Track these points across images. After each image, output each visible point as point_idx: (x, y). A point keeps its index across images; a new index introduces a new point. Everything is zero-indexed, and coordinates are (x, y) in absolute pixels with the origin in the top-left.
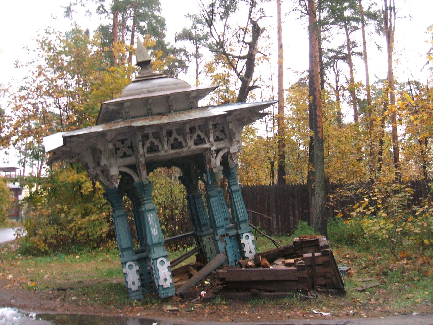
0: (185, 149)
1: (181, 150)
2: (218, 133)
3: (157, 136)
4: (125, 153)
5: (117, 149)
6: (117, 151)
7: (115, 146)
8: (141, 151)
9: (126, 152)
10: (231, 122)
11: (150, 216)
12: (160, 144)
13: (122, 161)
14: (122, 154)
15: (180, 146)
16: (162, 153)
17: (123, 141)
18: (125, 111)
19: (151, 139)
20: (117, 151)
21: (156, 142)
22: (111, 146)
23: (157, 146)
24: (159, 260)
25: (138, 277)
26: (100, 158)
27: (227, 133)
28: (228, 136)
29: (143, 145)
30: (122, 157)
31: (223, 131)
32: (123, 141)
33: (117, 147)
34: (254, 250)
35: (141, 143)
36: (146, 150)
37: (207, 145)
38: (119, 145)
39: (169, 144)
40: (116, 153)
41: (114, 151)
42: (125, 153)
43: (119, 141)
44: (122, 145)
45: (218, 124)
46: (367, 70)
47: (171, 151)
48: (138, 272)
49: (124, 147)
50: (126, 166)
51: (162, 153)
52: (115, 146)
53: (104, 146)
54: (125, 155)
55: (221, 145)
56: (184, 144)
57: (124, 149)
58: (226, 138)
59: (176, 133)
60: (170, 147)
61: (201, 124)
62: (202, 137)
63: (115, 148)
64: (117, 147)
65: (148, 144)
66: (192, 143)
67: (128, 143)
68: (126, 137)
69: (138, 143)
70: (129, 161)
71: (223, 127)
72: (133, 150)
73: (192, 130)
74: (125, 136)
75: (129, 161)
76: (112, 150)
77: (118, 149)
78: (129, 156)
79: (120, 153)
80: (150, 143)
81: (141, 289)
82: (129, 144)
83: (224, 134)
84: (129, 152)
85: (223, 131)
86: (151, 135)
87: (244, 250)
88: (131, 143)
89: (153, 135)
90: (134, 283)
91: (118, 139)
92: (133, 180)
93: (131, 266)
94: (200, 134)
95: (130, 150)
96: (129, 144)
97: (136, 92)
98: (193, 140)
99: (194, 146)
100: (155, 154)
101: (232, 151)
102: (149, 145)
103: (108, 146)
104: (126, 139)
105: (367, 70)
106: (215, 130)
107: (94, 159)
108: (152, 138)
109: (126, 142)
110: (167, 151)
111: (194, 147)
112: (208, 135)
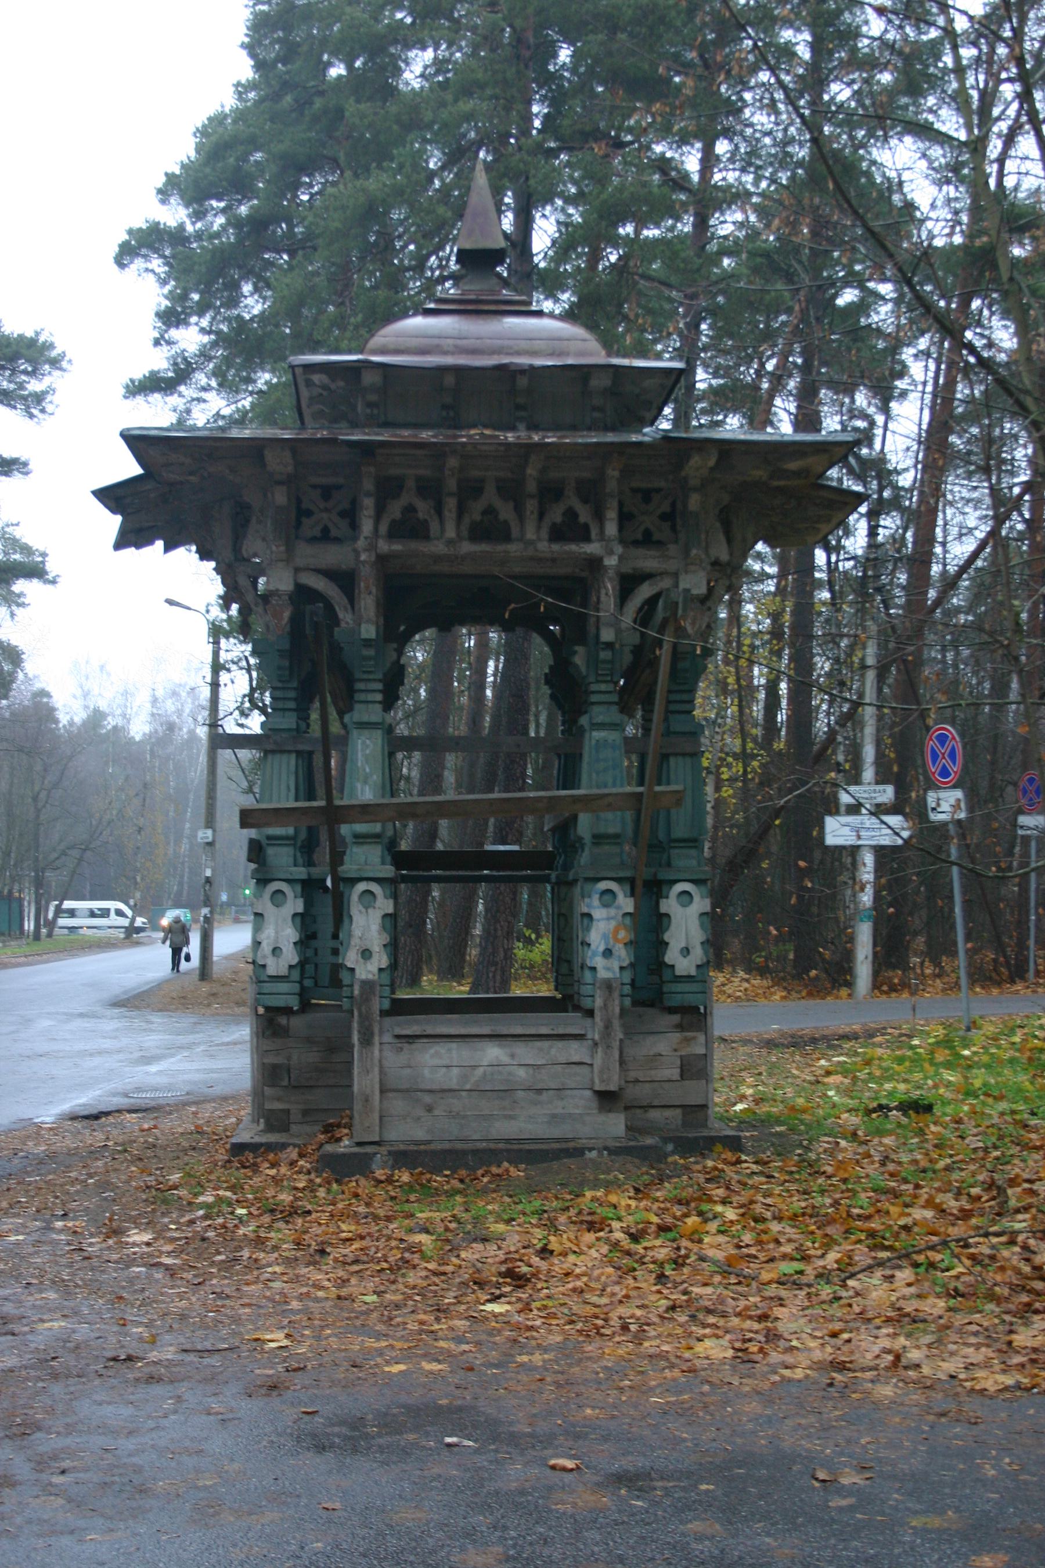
0: (513, 548)
1: (500, 548)
3: (511, 491)
4: (326, 530)
5: (303, 513)
7: (299, 501)
8: (367, 526)
9: (330, 525)
11: (364, 743)
13: (307, 554)
14: (317, 532)
16: (438, 547)
19: (490, 496)
20: (304, 520)
21: (424, 509)
23: (506, 522)
24: (362, 887)
30: (313, 540)
32: (327, 492)
33: (304, 506)
36: (383, 529)
37: (593, 548)
42: (326, 530)
43: (314, 487)
45: (658, 490)
47: (467, 547)
48: (298, 920)
49: (327, 510)
50: (318, 571)
52: (299, 501)
54: (325, 536)
55: (647, 561)
56: (515, 532)
57: (325, 515)
58: (676, 542)
60: (465, 533)
62: (582, 519)
64: (304, 506)
65: (395, 510)
66: (544, 533)
68: (341, 481)
70: (333, 556)
73: (550, 492)
75: (333, 556)
77: (309, 513)
78: (337, 540)
79: (310, 527)
80: (485, 513)
81: (296, 975)
86: (411, 484)
90: (686, 951)
92: (335, 621)
93: (280, 896)
94: (498, 503)
97: (414, 342)
100: (414, 545)
102: (559, 519)
104: (338, 487)
111: (543, 546)
112: (599, 516)
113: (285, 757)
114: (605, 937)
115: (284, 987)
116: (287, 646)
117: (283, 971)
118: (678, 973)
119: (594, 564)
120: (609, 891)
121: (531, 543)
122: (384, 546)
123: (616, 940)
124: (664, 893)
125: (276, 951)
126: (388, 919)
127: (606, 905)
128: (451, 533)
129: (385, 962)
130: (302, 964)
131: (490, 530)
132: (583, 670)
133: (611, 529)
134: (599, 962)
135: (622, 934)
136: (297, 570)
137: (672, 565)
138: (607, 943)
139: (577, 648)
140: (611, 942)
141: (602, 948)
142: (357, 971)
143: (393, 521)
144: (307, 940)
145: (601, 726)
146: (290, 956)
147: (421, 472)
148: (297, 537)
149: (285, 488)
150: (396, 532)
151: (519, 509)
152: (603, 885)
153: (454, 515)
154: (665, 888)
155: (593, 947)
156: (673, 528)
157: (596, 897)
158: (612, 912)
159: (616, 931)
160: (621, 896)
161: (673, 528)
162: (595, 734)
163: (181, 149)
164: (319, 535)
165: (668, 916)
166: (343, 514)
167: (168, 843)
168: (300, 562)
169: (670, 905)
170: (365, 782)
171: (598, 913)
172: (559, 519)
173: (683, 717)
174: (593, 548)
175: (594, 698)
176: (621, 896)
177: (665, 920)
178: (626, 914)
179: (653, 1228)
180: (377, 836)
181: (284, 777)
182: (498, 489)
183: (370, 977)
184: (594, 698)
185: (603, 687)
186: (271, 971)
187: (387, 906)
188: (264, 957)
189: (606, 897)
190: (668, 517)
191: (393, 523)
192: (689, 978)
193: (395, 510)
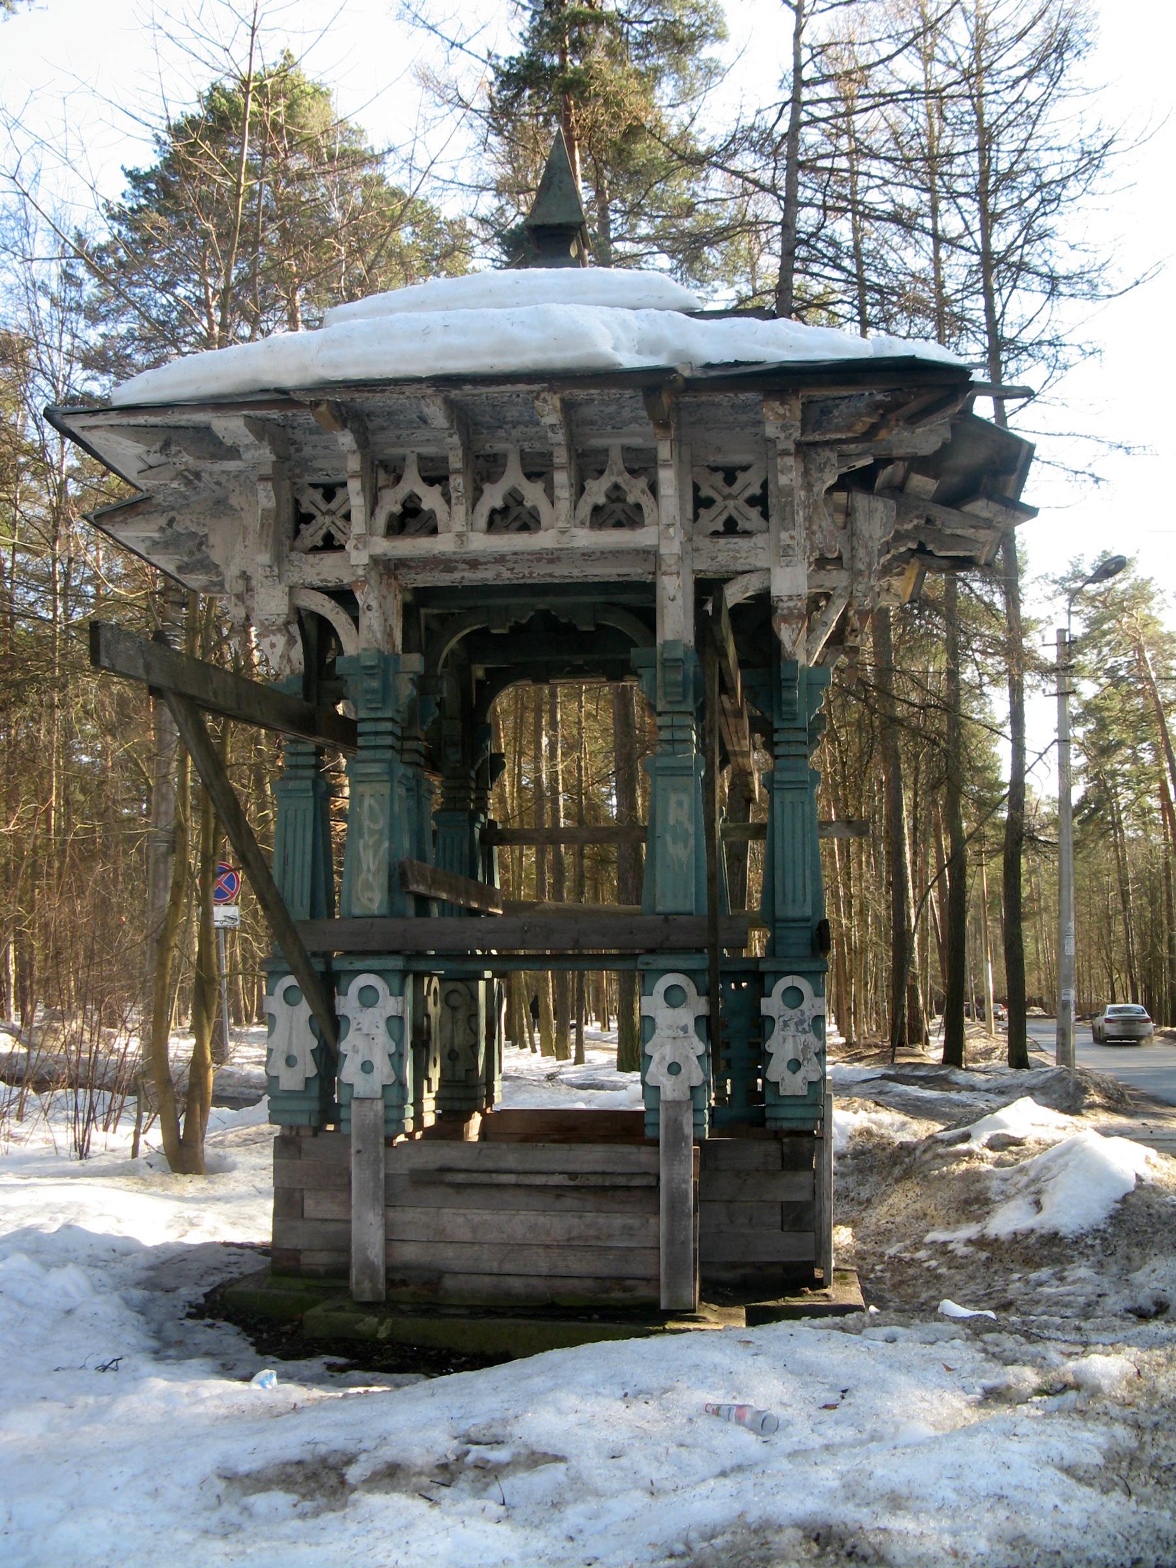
48: (703, 1024)
49: (331, 513)
79: (312, 534)
119: (651, 555)
124: (342, 987)
128: (458, 525)
143: (392, 516)
148: (292, 549)
149: (269, 485)
151: (549, 491)
154: (343, 981)
156: (765, 515)
161: (765, 515)
168: (295, 577)
169: (347, 1004)
172: (601, 500)
174: (642, 537)
179: (569, 1496)
187: (701, 1006)
190: (760, 501)
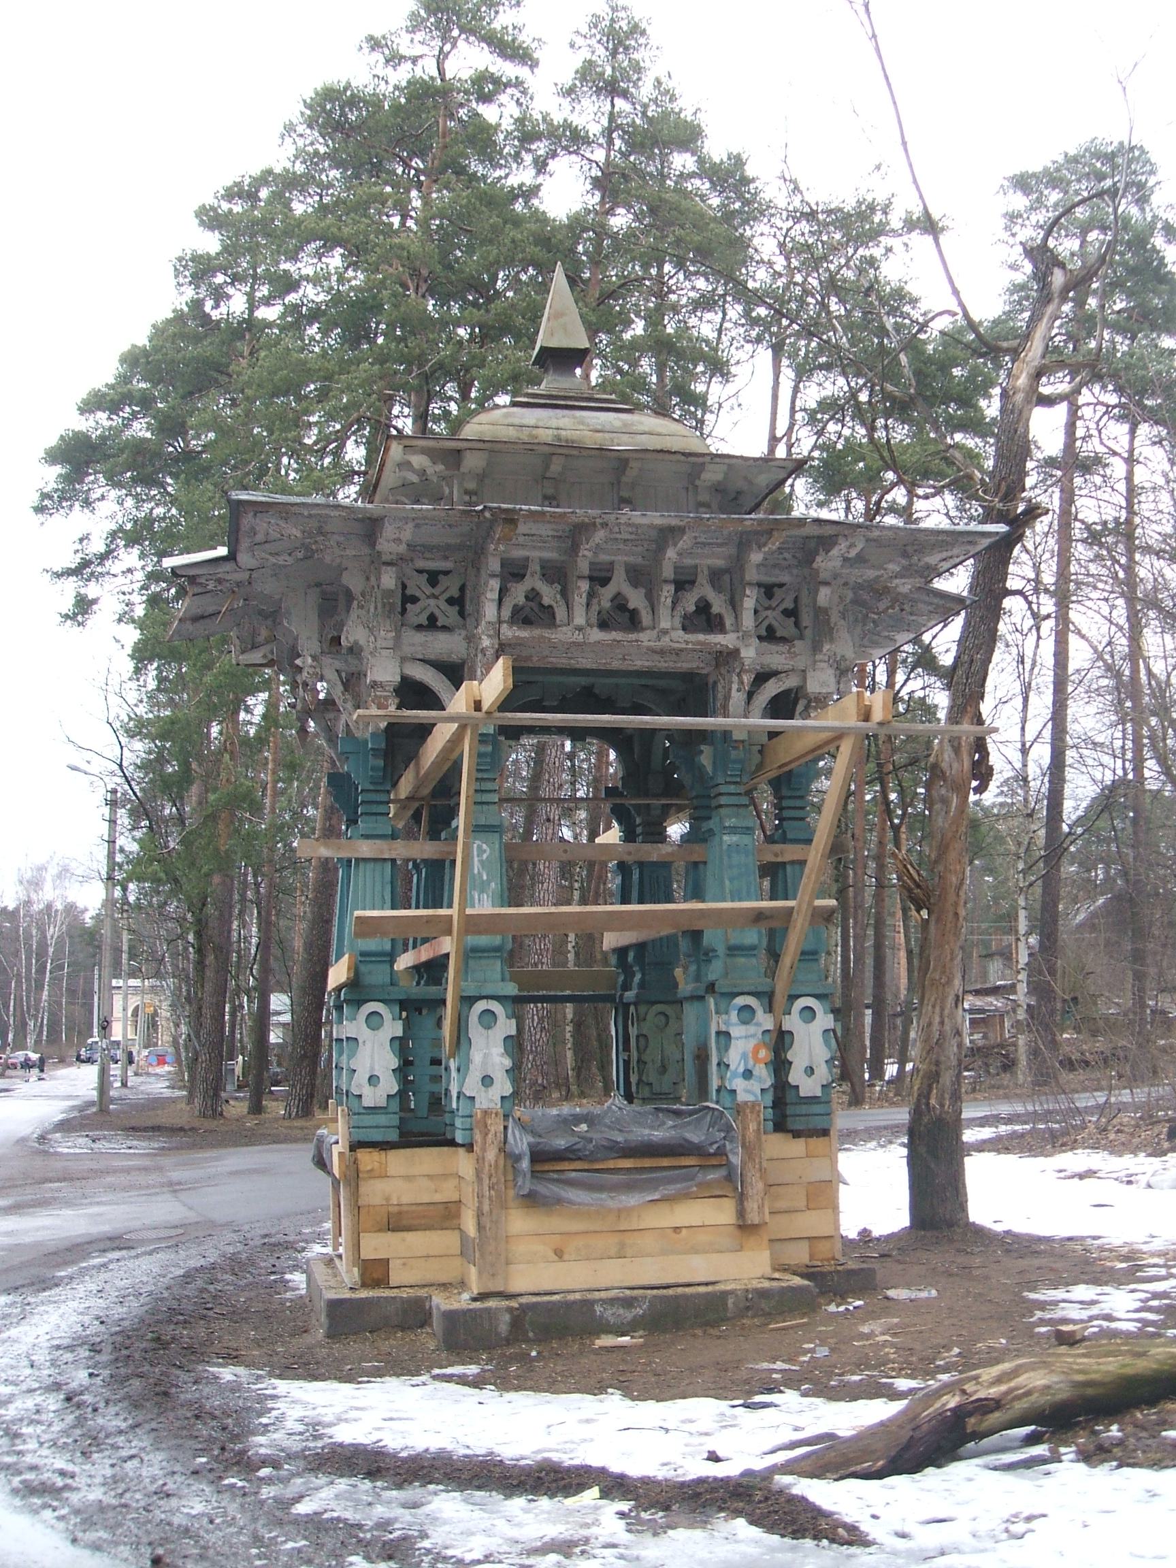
1: (633, 636)
2: (773, 617)
4: (432, 619)
6: (409, 606)
7: (404, 587)
8: (490, 611)
9: (437, 613)
10: (827, 584)
11: (479, 847)
12: (562, 603)
13: (416, 642)
14: (423, 619)
15: (632, 621)
17: (433, 578)
18: (460, 484)
19: (533, 581)
20: (409, 606)
22: (389, 580)
25: (394, 1063)
26: (341, 625)
27: (806, 619)
28: (808, 633)
29: (503, 592)
30: (419, 627)
31: (792, 613)
32: (433, 578)
33: (409, 592)
34: (824, 1066)
35: (495, 584)
36: (506, 613)
37: (726, 640)
38: (419, 584)
39: (595, 608)
40: (404, 611)
41: (398, 601)
42: (432, 619)
43: (420, 571)
44: (429, 590)
45: (781, 585)
46: (889, 85)
47: (596, 635)
48: (397, 1043)
49: (435, 597)
51: (563, 635)
52: (404, 587)
53: (368, 579)
54: (432, 624)
55: (776, 658)
56: (646, 618)
57: (432, 602)
58: (801, 637)
59: (624, 576)
60: (594, 620)
61: (720, 563)
62: (715, 609)
63: (403, 594)
65: (518, 594)
66: (677, 622)
67: (451, 586)
69: (486, 584)
71: (796, 600)
72: (462, 614)
74: (446, 558)
76: (389, 593)
77: (414, 600)
79: (417, 614)
81: (395, 1106)
82: (454, 592)
83: (797, 624)
84: (448, 615)
85: (792, 613)
86: (535, 567)
87: (789, 1057)
88: (462, 589)
89: (542, 567)
90: (810, 1071)
91: (421, 564)
93: (375, 1018)
95: (453, 611)
96: (454, 592)
98: (680, 611)
99: (681, 633)
101: (813, 687)
103: (378, 579)
105: (889, 85)
106: (766, 603)
107: (322, 626)
108: (537, 576)
109: (444, 581)
110: (580, 629)
112: (734, 604)
113: (378, 866)
114: (744, 1056)
115: (382, 1119)
116: (383, 746)
117: (382, 1102)
118: (802, 1094)
120: (747, 1008)
121: (665, 632)
122: (508, 632)
123: (756, 1060)
125: (373, 1080)
126: (510, 1042)
127: (744, 1022)
128: (579, 619)
129: (508, 1089)
130: (402, 1094)
131: (622, 617)
132: (709, 769)
133: (748, 620)
134: (739, 1084)
135: (763, 1053)
136: (403, 660)
137: (800, 662)
138: (746, 1063)
139: (703, 747)
140: (751, 1062)
141: (741, 1069)
142: (477, 1101)
144: (404, 1069)
145: (733, 830)
146: (390, 1085)
147: (547, 555)
150: (521, 617)
152: (740, 1001)
153: (584, 600)
155: (732, 1067)
157: (734, 1015)
158: (752, 1029)
159: (756, 1050)
160: (760, 1013)
162: (725, 838)
163: (104, 372)
164: (426, 623)
165: (791, 1033)
166: (451, 601)
167: (40, 987)
168: (407, 650)
170: (482, 891)
171: (736, 1031)
173: (796, 823)
175: (723, 800)
176: (760, 1013)
177: (787, 1037)
178: (765, 1032)
180: (497, 949)
181: (378, 888)
182: (627, 572)
183: (492, 1105)
184: (723, 800)
185: (732, 789)
186: (367, 1102)
188: (360, 1086)
189: (746, 1015)
191: (516, 610)
192: (813, 1100)
193: (518, 594)
